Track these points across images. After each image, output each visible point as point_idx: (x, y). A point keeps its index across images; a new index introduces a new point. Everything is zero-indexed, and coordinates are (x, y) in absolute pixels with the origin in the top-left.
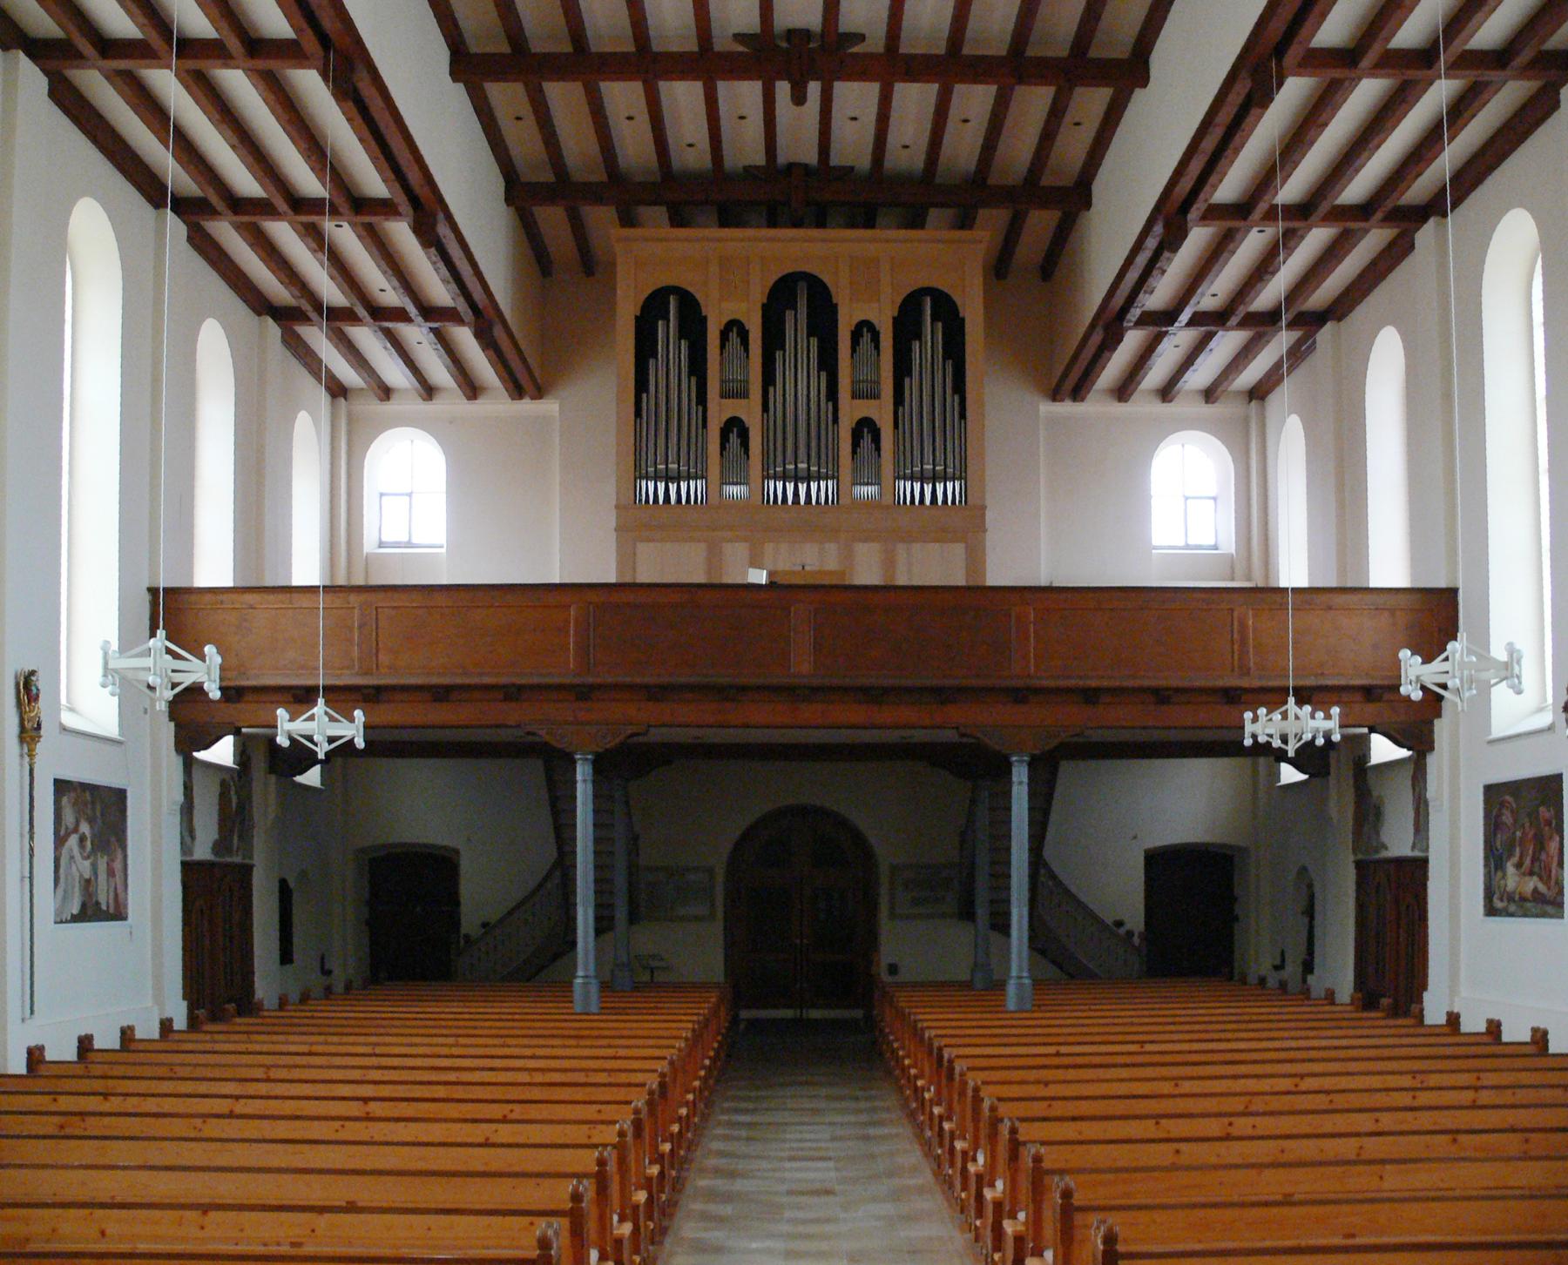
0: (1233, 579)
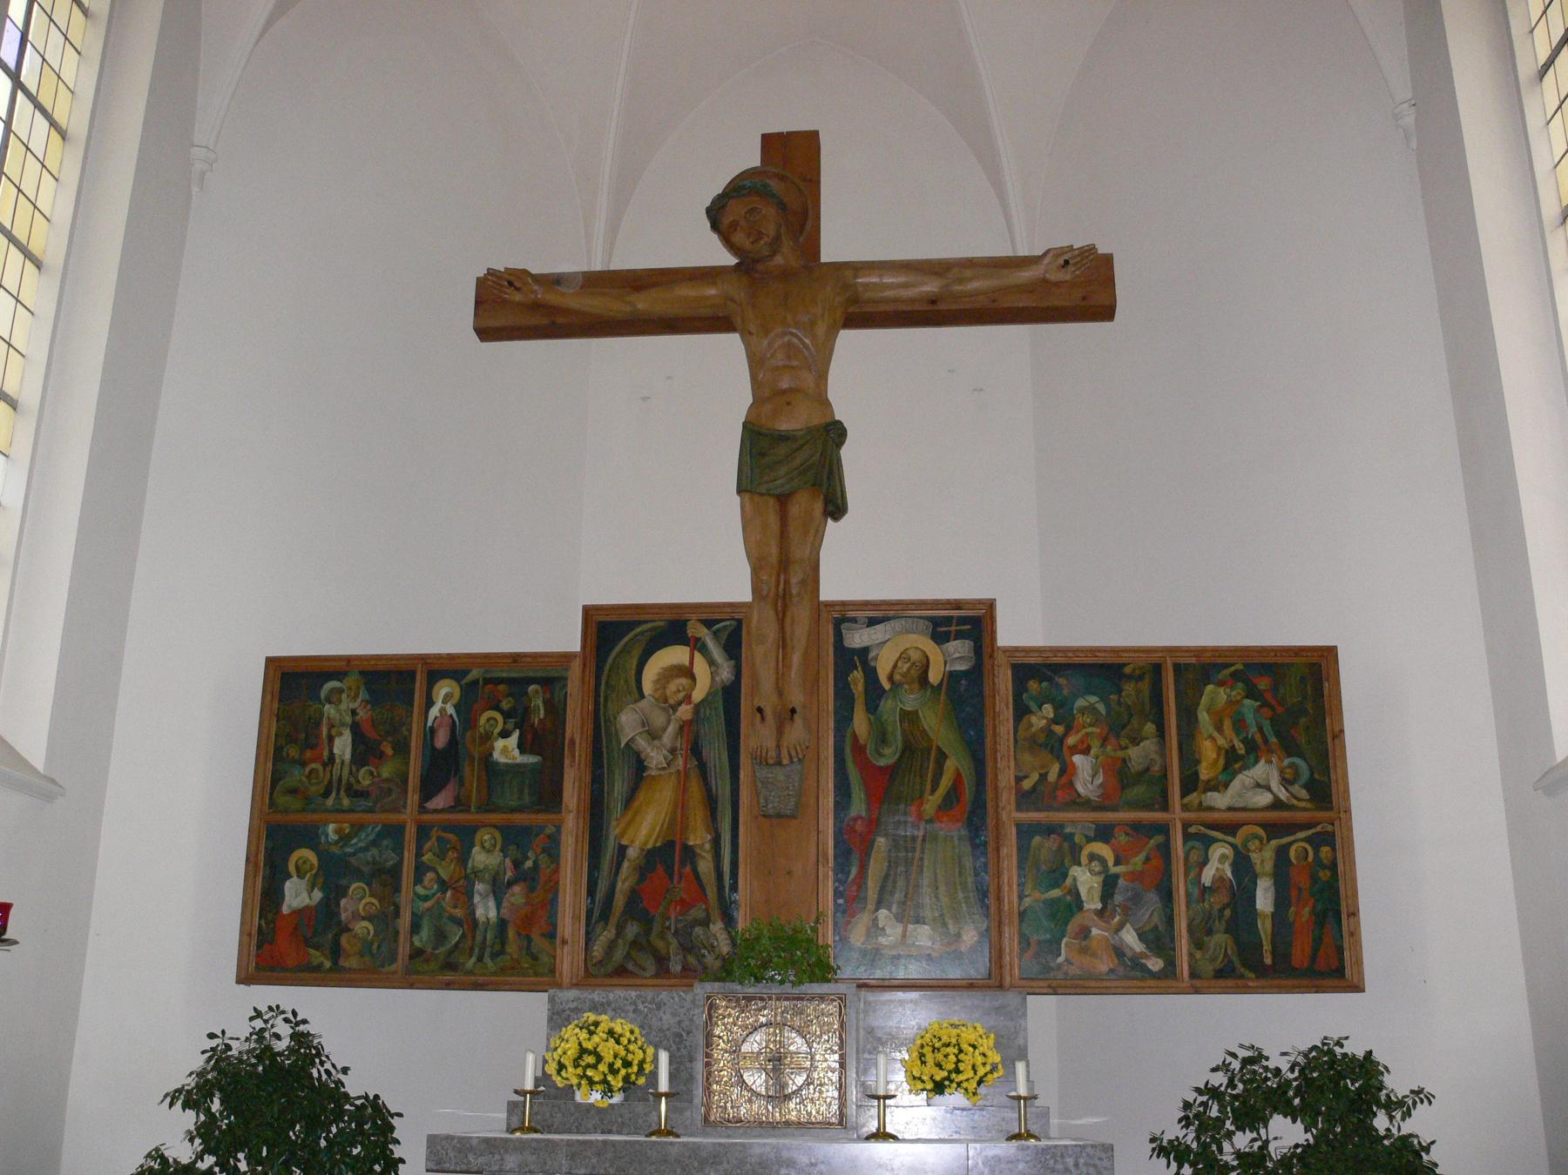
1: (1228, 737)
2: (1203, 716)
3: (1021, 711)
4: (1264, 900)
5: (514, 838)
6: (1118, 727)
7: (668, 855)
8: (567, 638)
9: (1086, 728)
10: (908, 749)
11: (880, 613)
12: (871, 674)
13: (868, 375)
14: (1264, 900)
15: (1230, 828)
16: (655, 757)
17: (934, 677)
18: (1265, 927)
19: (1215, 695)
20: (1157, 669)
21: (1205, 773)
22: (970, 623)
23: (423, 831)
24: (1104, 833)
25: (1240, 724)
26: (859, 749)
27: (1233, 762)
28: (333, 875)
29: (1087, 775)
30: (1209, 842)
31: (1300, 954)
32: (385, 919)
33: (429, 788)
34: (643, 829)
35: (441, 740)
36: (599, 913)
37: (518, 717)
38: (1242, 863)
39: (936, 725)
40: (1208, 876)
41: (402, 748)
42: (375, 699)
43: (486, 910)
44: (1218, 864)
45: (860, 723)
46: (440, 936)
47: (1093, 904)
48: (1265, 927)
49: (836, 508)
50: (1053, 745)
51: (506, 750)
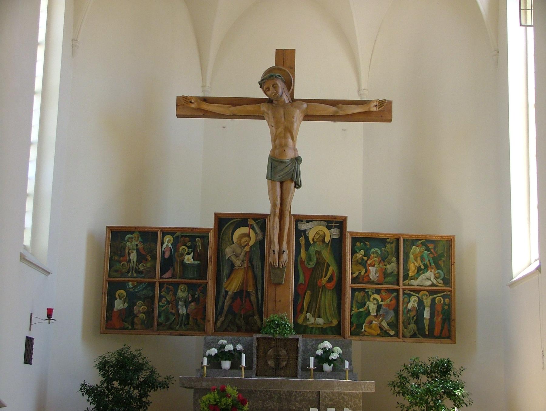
0: (354, 280)
1: (419, 263)
2: (411, 256)
3: (354, 252)
4: (427, 314)
5: (191, 287)
6: (384, 259)
7: (241, 294)
8: (210, 224)
9: (374, 259)
10: (318, 263)
11: (309, 219)
12: (307, 238)
13: (312, 140)
14: (427, 314)
15: (418, 291)
16: (238, 263)
17: (327, 240)
18: (426, 323)
19: (416, 249)
20: (398, 240)
21: (411, 274)
22: (339, 223)
23: (162, 284)
24: (378, 291)
25: (422, 259)
26: (302, 262)
27: (420, 271)
28: (131, 298)
29: (373, 273)
30: (410, 296)
31: (437, 331)
32: (149, 313)
33: (163, 272)
34: (233, 285)
35: (167, 255)
36: (218, 313)
37: (192, 248)
38: (421, 303)
39: (327, 255)
40: (410, 306)
41: (154, 258)
42: (144, 241)
43: (182, 311)
44: (413, 303)
45: (303, 254)
46: (167, 319)
47: (373, 313)
48: (426, 323)
49: (298, 185)
50: (363, 263)
51: (189, 259)
